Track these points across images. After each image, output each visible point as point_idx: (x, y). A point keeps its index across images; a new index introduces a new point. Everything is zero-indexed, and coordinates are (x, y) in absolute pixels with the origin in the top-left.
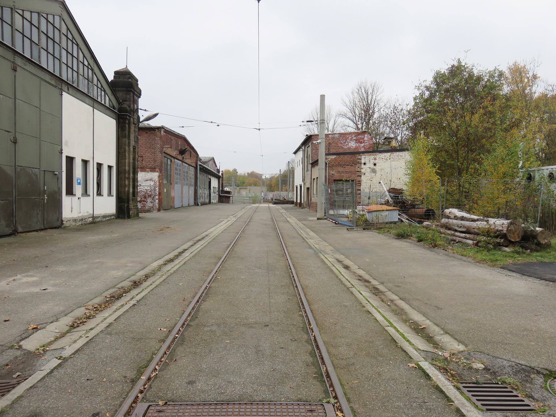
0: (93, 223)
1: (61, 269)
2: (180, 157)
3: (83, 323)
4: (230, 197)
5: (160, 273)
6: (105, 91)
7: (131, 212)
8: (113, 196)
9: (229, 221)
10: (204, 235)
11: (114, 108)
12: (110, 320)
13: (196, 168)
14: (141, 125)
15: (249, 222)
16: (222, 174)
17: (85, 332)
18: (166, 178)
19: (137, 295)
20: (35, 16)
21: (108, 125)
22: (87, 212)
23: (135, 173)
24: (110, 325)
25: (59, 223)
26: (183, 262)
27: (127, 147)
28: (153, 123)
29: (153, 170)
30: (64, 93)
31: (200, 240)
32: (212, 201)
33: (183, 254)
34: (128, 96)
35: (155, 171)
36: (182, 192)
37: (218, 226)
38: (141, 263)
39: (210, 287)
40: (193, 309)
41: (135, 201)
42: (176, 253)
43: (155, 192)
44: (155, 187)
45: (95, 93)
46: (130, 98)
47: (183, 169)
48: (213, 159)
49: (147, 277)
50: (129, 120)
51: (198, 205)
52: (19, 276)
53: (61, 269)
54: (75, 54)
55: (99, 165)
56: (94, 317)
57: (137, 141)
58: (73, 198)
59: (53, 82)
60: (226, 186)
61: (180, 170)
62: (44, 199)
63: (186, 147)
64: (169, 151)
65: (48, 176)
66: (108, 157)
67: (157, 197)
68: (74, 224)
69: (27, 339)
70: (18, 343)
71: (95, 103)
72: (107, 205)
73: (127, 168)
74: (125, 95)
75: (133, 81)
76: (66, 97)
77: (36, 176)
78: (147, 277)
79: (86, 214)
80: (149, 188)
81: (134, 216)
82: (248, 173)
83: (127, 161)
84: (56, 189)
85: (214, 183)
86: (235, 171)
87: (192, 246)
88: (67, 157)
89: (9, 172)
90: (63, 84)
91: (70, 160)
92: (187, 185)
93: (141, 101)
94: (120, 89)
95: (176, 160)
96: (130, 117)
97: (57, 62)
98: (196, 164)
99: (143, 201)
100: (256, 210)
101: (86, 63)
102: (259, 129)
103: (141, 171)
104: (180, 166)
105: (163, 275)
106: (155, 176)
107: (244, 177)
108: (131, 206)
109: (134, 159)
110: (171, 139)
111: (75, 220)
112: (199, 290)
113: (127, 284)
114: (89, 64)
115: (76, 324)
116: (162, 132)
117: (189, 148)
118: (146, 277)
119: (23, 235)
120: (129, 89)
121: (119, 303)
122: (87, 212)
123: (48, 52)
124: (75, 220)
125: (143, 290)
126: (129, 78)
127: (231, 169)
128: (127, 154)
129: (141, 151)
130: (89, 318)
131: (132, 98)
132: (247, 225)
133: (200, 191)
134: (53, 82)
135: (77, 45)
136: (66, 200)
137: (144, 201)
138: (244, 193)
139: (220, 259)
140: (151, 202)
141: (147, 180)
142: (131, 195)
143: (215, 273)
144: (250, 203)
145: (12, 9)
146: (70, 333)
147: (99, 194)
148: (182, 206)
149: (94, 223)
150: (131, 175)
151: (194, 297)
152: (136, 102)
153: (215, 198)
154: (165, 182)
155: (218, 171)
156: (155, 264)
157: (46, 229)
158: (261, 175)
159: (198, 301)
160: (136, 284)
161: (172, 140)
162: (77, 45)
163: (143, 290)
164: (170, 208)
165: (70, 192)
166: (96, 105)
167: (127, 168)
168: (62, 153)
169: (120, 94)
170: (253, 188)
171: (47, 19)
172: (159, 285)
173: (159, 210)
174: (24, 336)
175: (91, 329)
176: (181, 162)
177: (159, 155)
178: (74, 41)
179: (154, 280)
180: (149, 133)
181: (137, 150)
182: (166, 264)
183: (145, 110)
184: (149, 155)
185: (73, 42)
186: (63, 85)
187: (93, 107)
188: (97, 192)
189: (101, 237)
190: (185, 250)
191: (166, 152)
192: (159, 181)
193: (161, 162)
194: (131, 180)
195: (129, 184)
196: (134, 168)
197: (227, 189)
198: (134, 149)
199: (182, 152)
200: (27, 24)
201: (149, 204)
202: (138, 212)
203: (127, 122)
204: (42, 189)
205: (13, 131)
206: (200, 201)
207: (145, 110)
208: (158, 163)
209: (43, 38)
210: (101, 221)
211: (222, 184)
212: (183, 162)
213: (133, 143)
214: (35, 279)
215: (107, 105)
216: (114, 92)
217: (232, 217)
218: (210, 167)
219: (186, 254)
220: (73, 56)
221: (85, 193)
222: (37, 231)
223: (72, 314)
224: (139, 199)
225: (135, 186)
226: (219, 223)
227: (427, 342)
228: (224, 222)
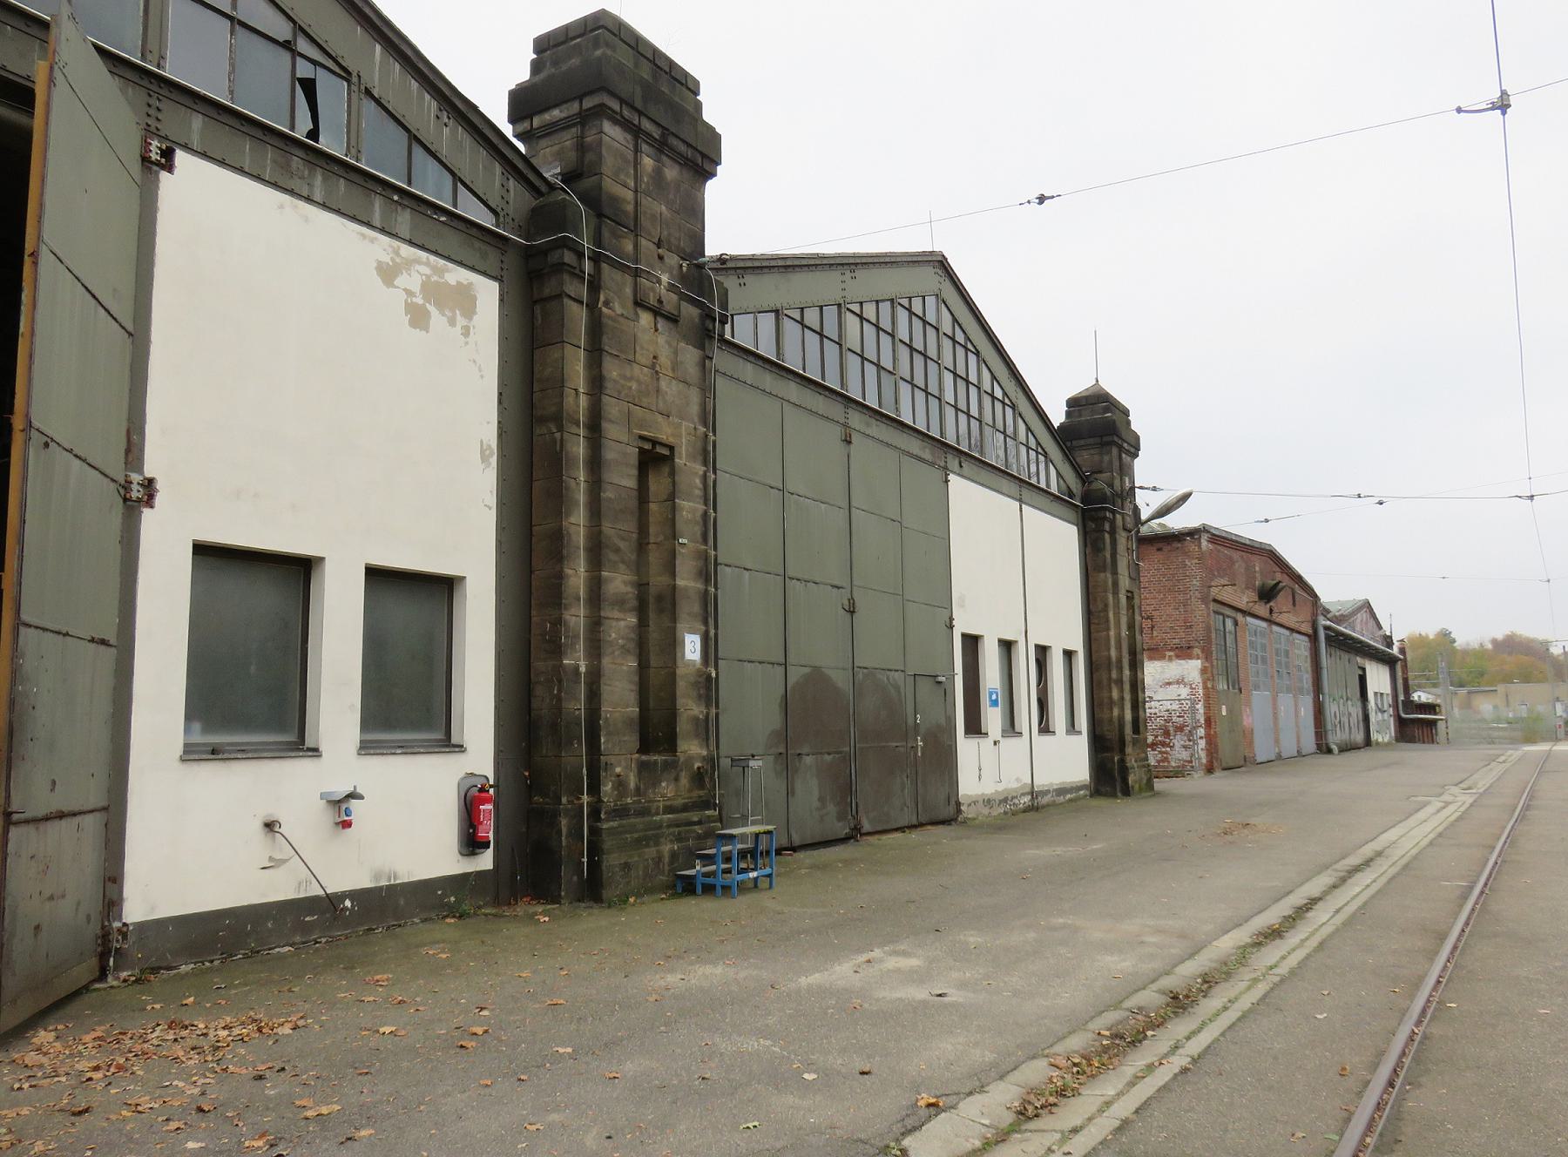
0: (1032, 808)
1: (973, 939)
2: (1262, 609)
3: (1049, 1107)
4: (1433, 723)
5: (1246, 975)
6: (1046, 455)
7: (1131, 779)
8: (1080, 733)
9: (1447, 804)
10: (1368, 850)
11: (1071, 495)
12: (1124, 1108)
13: (1314, 638)
14: (1144, 530)
15: (1527, 807)
16: (1402, 651)
17: (1058, 1136)
18: (1226, 675)
19: (1188, 1038)
20: (885, 308)
21: (1058, 540)
22: (1018, 780)
23: (1136, 666)
24: (1124, 1125)
26: (1313, 943)
27: (1110, 597)
28: (1176, 522)
29: (1184, 652)
30: (951, 477)
31: (1357, 869)
32: (1375, 736)
33: (1310, 914)
34: (1106, 458)
35: (1190, 657)
36: (1276, 713)
37: (1412, 821)
38: (1182, 936)
39: (1425, 1037)
40: (1379, 1107)
41: (1141, 744)
42: (1285, 908)
43: (1194, 718)
44: (1194, 703)
45: (1023, 462)
46: (1111, 462)
47: (1274, 646)
48: (1367, 606)
49: (1208, 982)
51: (1329, 751)
52: (877, 953)
53: (971, 939)
54: (973, 378)
55: (1042, 651)
56: (1076, 1093)
57: (1135, 577)
60: (1420, 687)
61: (1264, 647)
62: (914, 748)
63: (1279, 576)
64: (1227, 595)
65: (925, 687)
66: (1064, 627)
67: (1201, 732)
68: (986, 811)
69: (917, 1133)
70: (897, 1140)
71: (1023, 488)
72: (1066, 759)
73: (1113, 653)
74: (1097, 458)
75: (1117, 417)
76: (959, 487)
77: (897, 688)
78: (1208, 982)
79: (1015, 785)
80: (1175, 706)
81: (1141, 790)
82: (1494, 642)
83: (1112, 633)
84: (943, 721)
85: (1378, 679)
86: (1445, 636)
87: (1335, 887)
88: (964, 636)
89: (840, 684)
90: (949, 455)
91: (972, 643)
92: (1289, 690)
93: (1138, 464)
94: (1082, 442)
95: (1249, 619)
96: (1113, 512)
97: (934, 403)
99: (1164, 743)
100: (1544, 766)
101: (998, 393)
102: (1532, 497)
103: (1151, 658)
104: (1263, 634)
105: (1255, 981)
106: (1191, 668)
107: (1480, 654)
108: (1131, 762)
109: (1131, 627)
110: (1231, 558)
112: (1388, 1042)
113: (1150, 998)
114: (1005, 394)
115: (1030, 1109)
116: (1204, 543)
117: (1286, 581)
118: (1205, 982)
119: (873, 839)
120: (1106, 439)
121: (1137, 1060)
122: (1018, 780)
123: (914, 386)
124: (988, 802)
125: (1204, 1024)
126: (1107, 410)
127: (1431, 631)
128: (1111, 615)
129: (1148, 601)
130: (1061, 1093)
131: (1116, 464)
132: (1522, 818)
133: (1331, 709)
134: (927, 455)
135: (977, 354)
136: (966, 748)
137: (1164, 744)
138: (1486, 706)
139: (1442, 937)
140: (1185, 747)
141: (1170, 684)
142: (1128, 729)
143: (1435, 989)
144: (1514, 741)
145: (839, 305)
146: (1019, 1132)
147: (1045, 728)
148: (1279, 757)
149: (1033, 810)
150: (1127, 672)
151: (1374, 1067)
152: (1126, 471)
153: (1383, 729)
154: (1222, 686)
155: (1388, 641)
156: (1227, 944)
157: (921, 825)
158: (1545, 645)
159: (1391, 1084)
160: (1179, 1003)
161: (1233, 563)
162: (977, 354)
163: (1204, 1024)
164: (1243, 763)
165: (974, 727)
166: (1026, 494)
167: (1113, 653)
168: (952, 627)
169: (1085, 457)
170: (1518, 689)
171: (909, 310)
172: (1250, 1011)
173: (1210, 770)
174: (909, 1123)
175: (1075, 1131)
176: (1264, 624)
177: (1200, 611)
178: (970, 346)
179: (1232, 995)
180: (1166, 548)
181: (1136, 601)
182: (1259, 944)
183: (1154, 489)
185: (967, 349)
186: (950, 457)
187: (1020, 501)
188: (1040, 723)
189: (1059, 850)
190: (1314, 901)
191: (1219, 598)
192: (1204, 683)
193: (1208, 629)
194: (1127, 687)
195: (1122, 698)
196: (1133, 653)
197: (1420, 696)
198: (1130, 598)
199: (1267, 594)
200: (869, 330)
201: (1179, 754)
202: (1151, 775)
203: (1107, 527)
204: (910, 721)
205: (846, 584)
206: (1335, 738)
207: (1154, 489)
208: (1198, 631)
209: (904, 353)
210: (1053, 805)
211: (1406, 680)
212: (1270, 622)
213: (1125, 582)
214: (914, 962)
215: (1054, 489)
216: (1068, 453)
217: (1455, 790)
218: (1359, 631)
219: (1321, 915)
220: (968, 382)
221: (1011, 728)
222: (901, 829)
223: (1016, 1076)
224: (1150, 739)
225: (1137, 705)
226: (1415, 811)
228: (1430, 809)
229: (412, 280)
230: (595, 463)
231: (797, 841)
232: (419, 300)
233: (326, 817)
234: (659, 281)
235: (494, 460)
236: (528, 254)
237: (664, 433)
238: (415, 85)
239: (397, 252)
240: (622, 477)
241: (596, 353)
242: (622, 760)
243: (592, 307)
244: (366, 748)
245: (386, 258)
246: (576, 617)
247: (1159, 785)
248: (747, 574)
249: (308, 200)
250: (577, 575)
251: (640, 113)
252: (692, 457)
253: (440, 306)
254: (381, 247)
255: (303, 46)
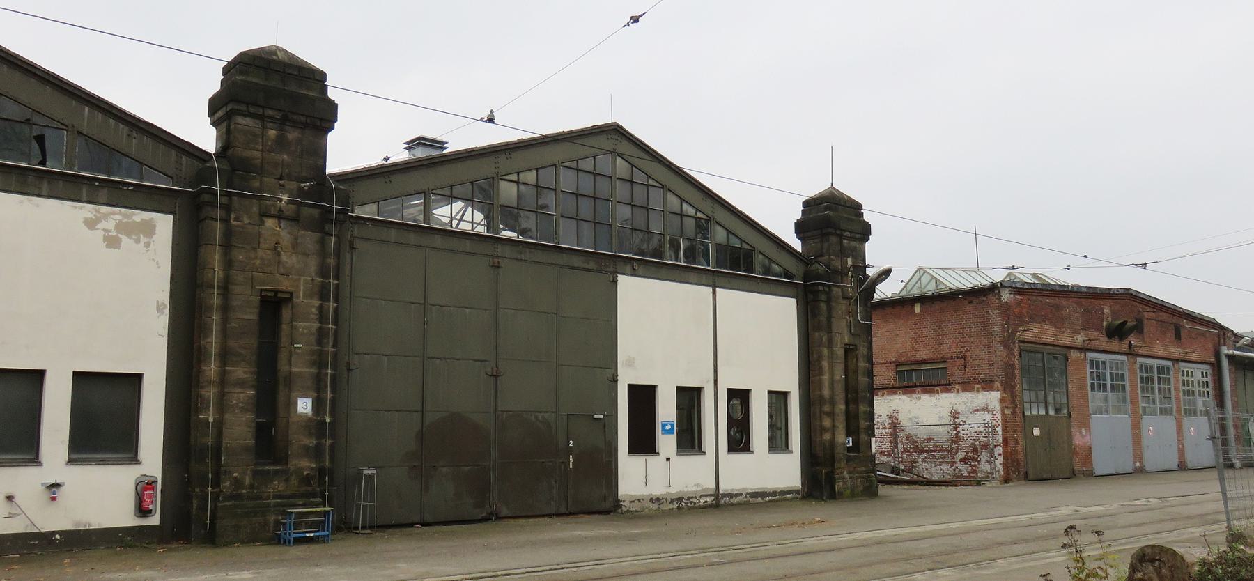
11: (787, 274)
25: (608, 504)
29: (987, 385)
50: (829, 294)
58: (651, 459)
59: (592, 265)
67: (999, 450)
79: (694, 489)
98: (1217, 354)
111: (658, 500)
134: (592, 265)
137: (973, 459)
173: (1006, 480)
180: (976, 301)
184: (977, 351)
203: (823, 297)
208: (999, 368)
227: (208, 553)
229: (110, 224)
230: (225, 308)
231: (428, 518)
232: (114, 234)
233: (46, 495)
234: (281, 200)
235: (167, 311)
236: (194, 196)
237: (284, 285)
238: (112, 122)
239: (98, 211)
240: (247, 314)
241: (227, 247)
242: (240, 472)
243: (225, 221)
244: (71, 461)
245: (90, 216)
246: (210, 392)
247: (883, 490)
248: (385, 358)
249: (39, 195)
250: (212, 369)
251: (263, 107)
252: (309, 295)
253: (129, 235)
254: (88, 210)
255: (36, 119)
